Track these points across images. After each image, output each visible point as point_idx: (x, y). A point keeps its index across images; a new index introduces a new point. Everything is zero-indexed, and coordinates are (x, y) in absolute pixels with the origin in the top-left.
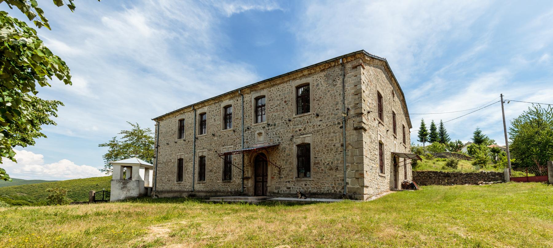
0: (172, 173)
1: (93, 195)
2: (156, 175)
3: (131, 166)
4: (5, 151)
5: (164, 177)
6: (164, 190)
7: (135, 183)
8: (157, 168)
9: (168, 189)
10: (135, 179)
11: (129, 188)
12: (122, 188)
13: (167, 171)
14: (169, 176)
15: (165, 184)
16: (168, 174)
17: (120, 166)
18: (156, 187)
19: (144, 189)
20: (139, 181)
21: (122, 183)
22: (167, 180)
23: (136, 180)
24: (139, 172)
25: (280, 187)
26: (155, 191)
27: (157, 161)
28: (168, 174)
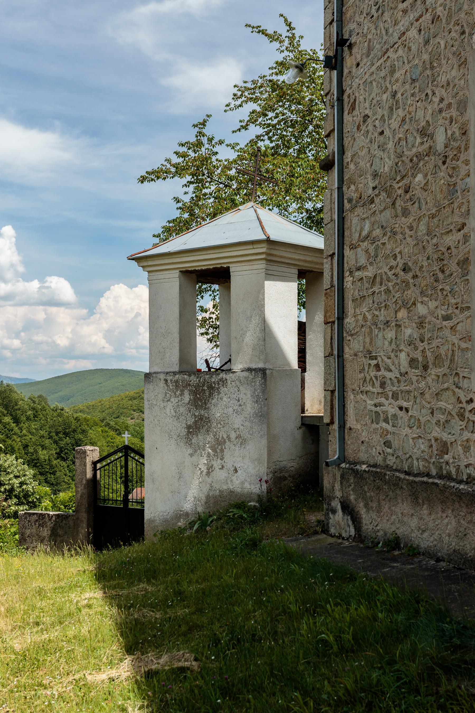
0: (143, 348)
1: (89, 474)
2: (341, 318)
3: (222, 263)
4: (233, 172)
5: (390, 334)
6: (391, 461)
7: (249, 393)
8: (347, 252)
9: (417, 453)
10: (246, 366)
11: (222, 434)
12: (189, 427)
13: (405, 269)
14: (421, 310)
15: (395, 396)
16: (412, 293)
17: (176, 274)
18: (342, 426)
19: (299, 434)
20: (263, 371)
21: (187, 397)
22: (413, 362)
23: (249, 370)
24: (263, 306)
25: (336, 554)
26: (337, 463)
27: (340, 188)
28: (412, 293)
